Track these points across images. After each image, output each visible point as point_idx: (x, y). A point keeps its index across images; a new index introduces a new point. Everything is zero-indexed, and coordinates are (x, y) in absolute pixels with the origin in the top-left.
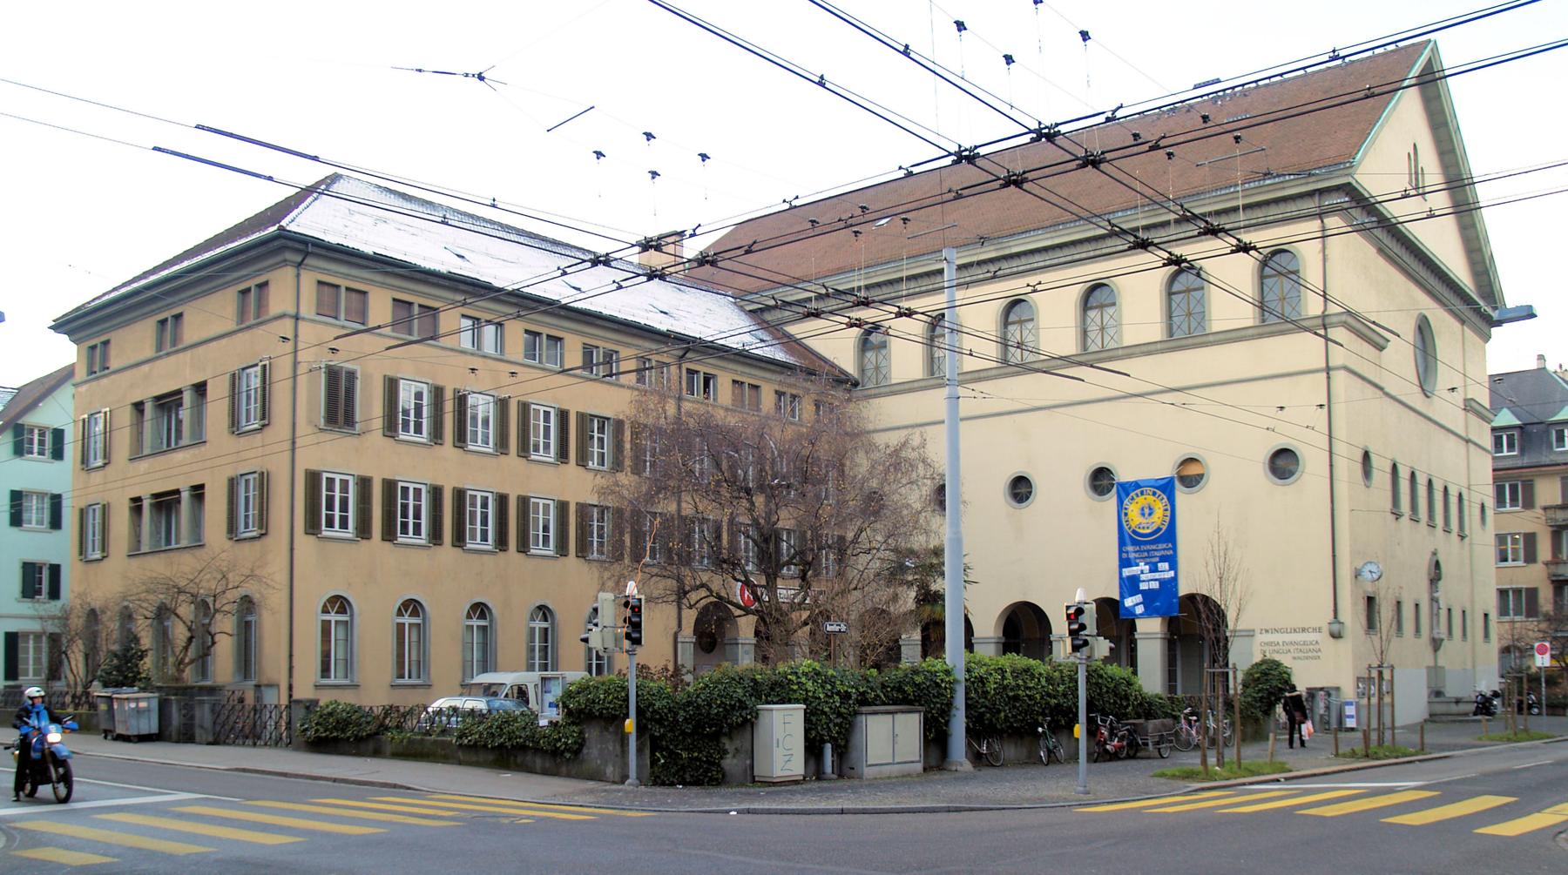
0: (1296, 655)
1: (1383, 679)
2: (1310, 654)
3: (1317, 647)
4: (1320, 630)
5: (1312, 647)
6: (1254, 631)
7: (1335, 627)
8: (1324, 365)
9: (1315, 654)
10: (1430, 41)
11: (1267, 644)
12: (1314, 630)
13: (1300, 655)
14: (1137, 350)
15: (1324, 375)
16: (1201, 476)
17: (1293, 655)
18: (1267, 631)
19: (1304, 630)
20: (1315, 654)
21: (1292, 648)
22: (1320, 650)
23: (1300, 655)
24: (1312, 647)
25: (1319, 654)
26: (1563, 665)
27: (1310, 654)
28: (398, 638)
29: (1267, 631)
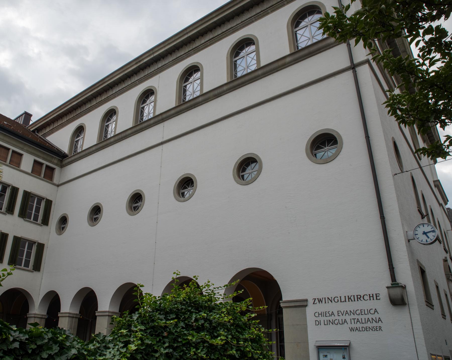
0: (353, 326)
1: (186, 30)
2: (369, 325)
3: (376, 316)
4: (377, 297)
5: (370, 316)
6: (306, 300)
7: (397, 292)
8: (252, 58)
9: (375, 324)
10: (183, 99)
11: (321, 314)
12: (371, 297)
13: (359, 325)
14: (212, 94)
15: (252, 59)
16: (307, 305)
17: (350, 326)
18: (320, 301)
19: (359, 298)
20: (375, 324)
21: (348, 318)
22: (380, 320)
23: (359, 325)
24: (370, 316)
25: (380, 324)
26: (426, 153)
27: (369, 325)
28: (253, 22)
29: (320, 301)
